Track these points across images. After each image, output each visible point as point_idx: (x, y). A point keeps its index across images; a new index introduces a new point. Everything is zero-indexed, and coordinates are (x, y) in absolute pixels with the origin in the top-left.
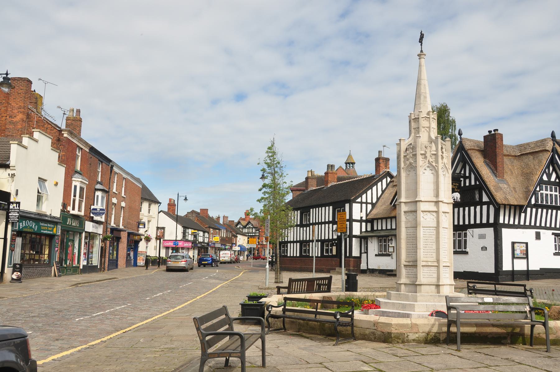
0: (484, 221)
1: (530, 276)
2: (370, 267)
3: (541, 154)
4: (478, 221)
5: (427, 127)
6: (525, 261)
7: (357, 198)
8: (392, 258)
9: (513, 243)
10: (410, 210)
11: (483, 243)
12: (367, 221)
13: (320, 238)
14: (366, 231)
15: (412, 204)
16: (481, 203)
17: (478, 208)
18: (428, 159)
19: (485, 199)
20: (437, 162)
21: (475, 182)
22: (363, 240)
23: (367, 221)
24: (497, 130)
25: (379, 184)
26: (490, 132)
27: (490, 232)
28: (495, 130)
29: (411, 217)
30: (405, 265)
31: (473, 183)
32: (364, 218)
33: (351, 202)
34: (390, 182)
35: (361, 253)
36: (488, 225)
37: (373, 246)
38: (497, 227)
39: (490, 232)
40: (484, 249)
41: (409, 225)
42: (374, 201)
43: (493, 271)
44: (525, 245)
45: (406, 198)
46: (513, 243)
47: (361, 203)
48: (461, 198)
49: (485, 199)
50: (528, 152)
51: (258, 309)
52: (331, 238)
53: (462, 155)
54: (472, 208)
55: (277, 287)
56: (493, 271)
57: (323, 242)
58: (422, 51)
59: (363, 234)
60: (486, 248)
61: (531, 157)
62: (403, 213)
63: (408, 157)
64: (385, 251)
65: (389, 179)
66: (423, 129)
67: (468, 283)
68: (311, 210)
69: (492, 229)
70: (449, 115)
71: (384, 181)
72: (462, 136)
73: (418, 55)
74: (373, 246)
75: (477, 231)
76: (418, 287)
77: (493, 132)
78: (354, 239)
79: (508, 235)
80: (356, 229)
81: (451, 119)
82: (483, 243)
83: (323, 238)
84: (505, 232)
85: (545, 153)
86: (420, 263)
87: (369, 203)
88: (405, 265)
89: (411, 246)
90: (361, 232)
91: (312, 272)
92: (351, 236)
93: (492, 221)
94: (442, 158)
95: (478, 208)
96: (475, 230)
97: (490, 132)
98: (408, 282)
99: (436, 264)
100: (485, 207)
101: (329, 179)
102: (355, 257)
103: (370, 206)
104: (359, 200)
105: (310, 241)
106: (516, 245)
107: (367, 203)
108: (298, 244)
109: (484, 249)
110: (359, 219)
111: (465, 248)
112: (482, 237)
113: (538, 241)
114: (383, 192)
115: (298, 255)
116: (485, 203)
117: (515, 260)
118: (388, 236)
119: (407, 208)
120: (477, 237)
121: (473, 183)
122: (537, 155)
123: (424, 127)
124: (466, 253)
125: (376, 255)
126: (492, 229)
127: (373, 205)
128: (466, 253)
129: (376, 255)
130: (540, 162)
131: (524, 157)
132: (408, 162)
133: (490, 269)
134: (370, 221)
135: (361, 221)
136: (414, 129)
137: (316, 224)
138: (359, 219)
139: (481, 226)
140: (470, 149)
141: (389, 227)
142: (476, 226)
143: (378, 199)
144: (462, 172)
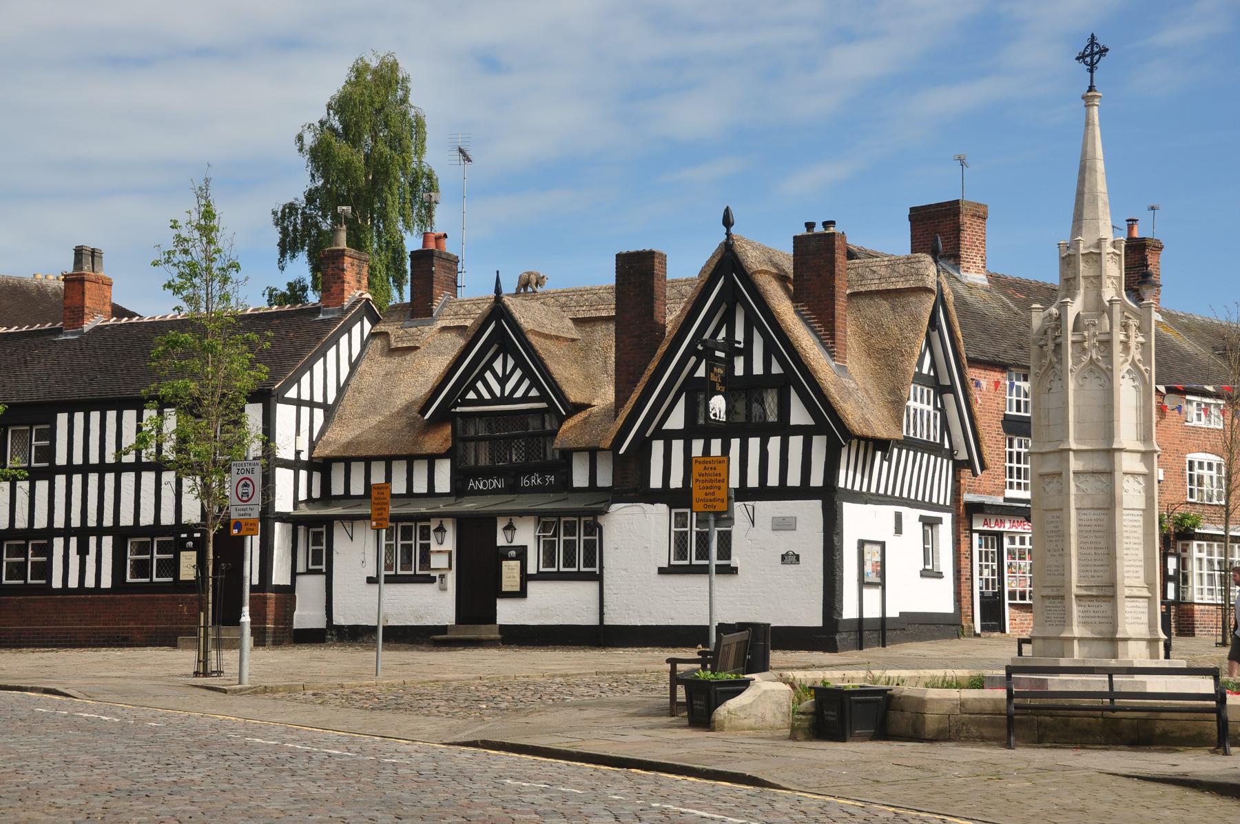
0: (794, 480)
1: (888, 634)
2: (339, 620)
3: (912, 299)
4: (773, 480)
5: (1115, 278)
6: (593, 587)
7: (287, 387)
8: (444, 589)
9: (862, 544)
10: (1089, 467)
11: (786, 541)
12: (311, 466)
13: (108, 521)
14: (310, 500)
15: (1096, 455)
16: (785, 429)
17: (774, 443)
18: (1132, 353)
19: (799, 415)
20: (1109, 358)
21: (767, 364)
22: (301, 530)
23: (311, 466)
24: (833, 223)
25: (344, 340)
26: (810, 226)
27: (812, 510)
28: (827, 224)
29: (1091, 485)
30: (1077, 596)
31: (758, 369)
32: (304, 457)
33: (267, 397)
34: (373, 335)
35: (294, 574)
36: (804, 492)
37: (356, 554)
38: (830, 499)
39: (812, 510)
40: (790, 558)
41: (1087, 503)
42: (330, 401)
43: (818, 622)
44: (878, 548)
45: (1077, 440)
46: (862, 544)
47: (298, 403)
48: (728, 412)
49: (799, 415)
50: (873, 288)
51: (878, 701)
52: (168, 518)
53: (730, 284)
54: (754, 443)
55: (668, 661)
56: (818, 622)
57: (121, 535)
58: (1091, 89)
59: (305, 511)
60: (797, 557)
61: (885, 305)
62: (1072, 475)
63: (1086, 344)
64: (407, 563)
65: (367, 326)
66: (1108, 281)
67: (673, 662)
68: (62, 418)
69: (816, 505)
70: (404, 101)
71: (356, 329)
72: (733, 230)
73: (1083, 98)
74: (356, 554)
75: (766, 509)
76: (1120, 644)
77: (819, 229)
78: (277, 525)
79: (859, 521)
80: (287, 492)
81: (412, 113)
82: (786, 541)
83: (127, 520)
84: (850, 511)
85: (924, 297)
86: (1123, 592)
87: (319, 405)
88: (1077, 596)
89: (1093, 551)
90: (296, 503)
91: (384, 627)
92: (268, 516)
93: (817, 480)
94: (1126, 346)
95: (774, 443)
96: (760, 505)
97: (810, 226)
98: (1088, 634)
99: (1145, 593)
100: (796, 443)
101: (88, 302)
102: (279, 589)
103: (319, 414)
104: (292, 393)
105: (50, 532)
106: (867, 548)
107: (312, 404)
108: (108, 541)
109: (790, 558)
110: (292, 458)
111: (725, 552)
112: (783, 525)
113: (897, 538)
114: (353, 366)
115: (106, 583)
116: (798, 430)
117: (865, 591)
118: (426, 517)
119: (1081, 463)
120: (769, 526)
121: (758, 369)
122: (904, 301)
123: (1109, 277)
124: (733, 571)
125: (662, 571)
126: (816, 505)
127: (329, 410)
128: (733, 571)
129: (662, 571)
130: (916, 320)
131: (864, 302)
132: (1086, 359)
133: (813, 617)
134: (319, 466)
135: (295, 465)
136: (1085, 278)
137: (85, 469)
138: (292, 458)
139: (783, 492)
140: (760, 272)
141: (420, 486)
142: (764, 493)
143: (340, 390)
144: (722, 334)
